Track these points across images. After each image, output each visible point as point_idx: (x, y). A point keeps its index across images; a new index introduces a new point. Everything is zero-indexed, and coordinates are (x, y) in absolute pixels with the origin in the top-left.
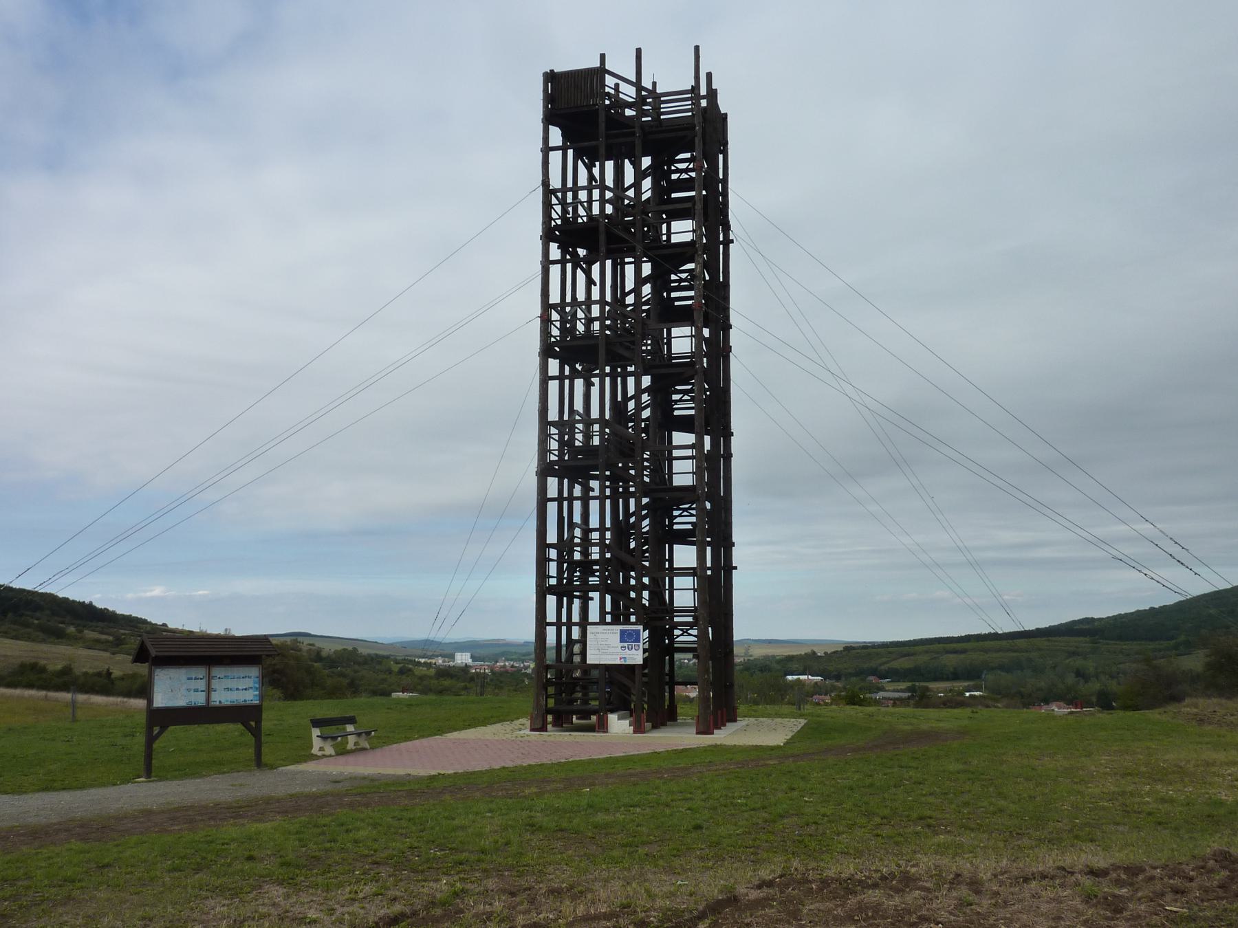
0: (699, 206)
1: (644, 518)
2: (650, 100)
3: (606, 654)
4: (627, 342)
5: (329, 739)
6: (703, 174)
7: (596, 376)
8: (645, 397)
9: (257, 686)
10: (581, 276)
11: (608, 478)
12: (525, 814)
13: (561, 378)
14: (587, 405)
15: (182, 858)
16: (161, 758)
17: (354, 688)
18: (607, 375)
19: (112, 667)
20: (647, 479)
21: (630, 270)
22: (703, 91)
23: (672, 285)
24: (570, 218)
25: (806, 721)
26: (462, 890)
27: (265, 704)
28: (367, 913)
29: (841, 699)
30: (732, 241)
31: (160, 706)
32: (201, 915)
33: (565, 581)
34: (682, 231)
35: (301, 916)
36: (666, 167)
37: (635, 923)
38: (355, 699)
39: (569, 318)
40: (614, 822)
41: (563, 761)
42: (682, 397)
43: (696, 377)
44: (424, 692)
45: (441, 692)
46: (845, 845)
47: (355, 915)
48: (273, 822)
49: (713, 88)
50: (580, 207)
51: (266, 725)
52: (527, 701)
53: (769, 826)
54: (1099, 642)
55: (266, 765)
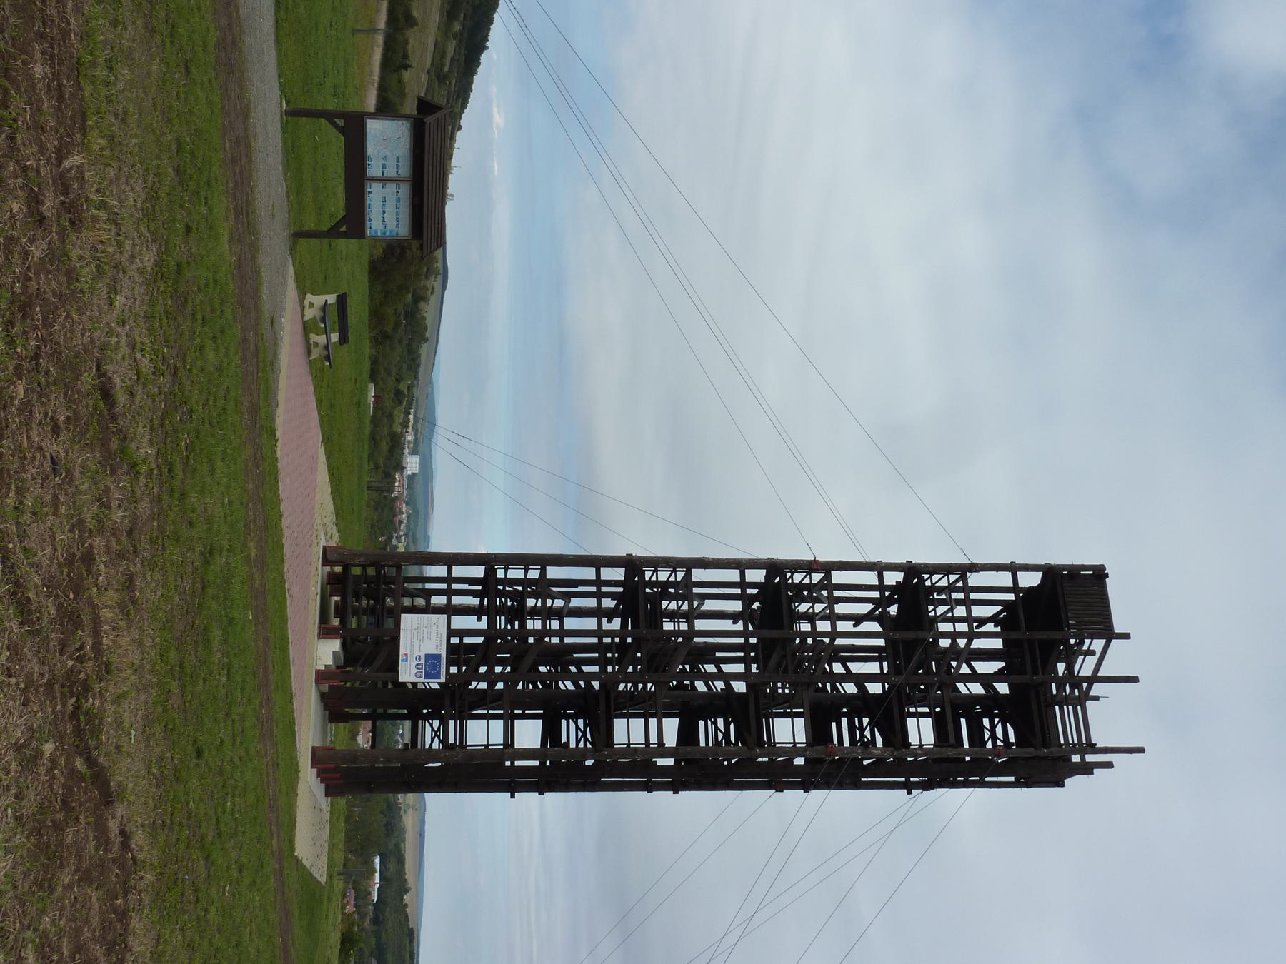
0: (951, 752)
1: (576, 684)
2: (1077, 693)
4: (787, 663)
5: (322, 314)
6: (990, 758)
7: (745, 626)
8: (720, 685)
9: (387, 234)
10: (865, 608)
11: (623, 640)
12: (226, 544)
13: (743, 584)
14: (710, 614)
15: (193, 153)
16: (308, 127)
17: (381, 338)
18: (747, 640)
19: (413, 70)
20: (621, 687)
21: (873, 667)
22: (1090, 758)
23: (856, 719)
24: (934, 596)
25: (323, 883)
26: (138, 473)
27: (365, 242)
28: (117, 363)
29: (349, 927)
30: (909, 793)
31: (368, 126)
32: (126, 176)
33: (501, 588)
34: (921, 731)
35: (118, 288)
36: (997, 711)
37: (86, 680)
38: (368, 340)
39: (814, 594)
40: (211, 651)
41: (287, 585)
42: (721, 731)
43: (745, 748)
44: (375, 421)
45: (373, 437)
46: (169, 940)
47: (116, 349)
48: (228, 252)
49: (1095, 770)
50: (947, 607)
51: (342, 243)
52: (358, 542)
53: (197, 841)
55: (295, 243)
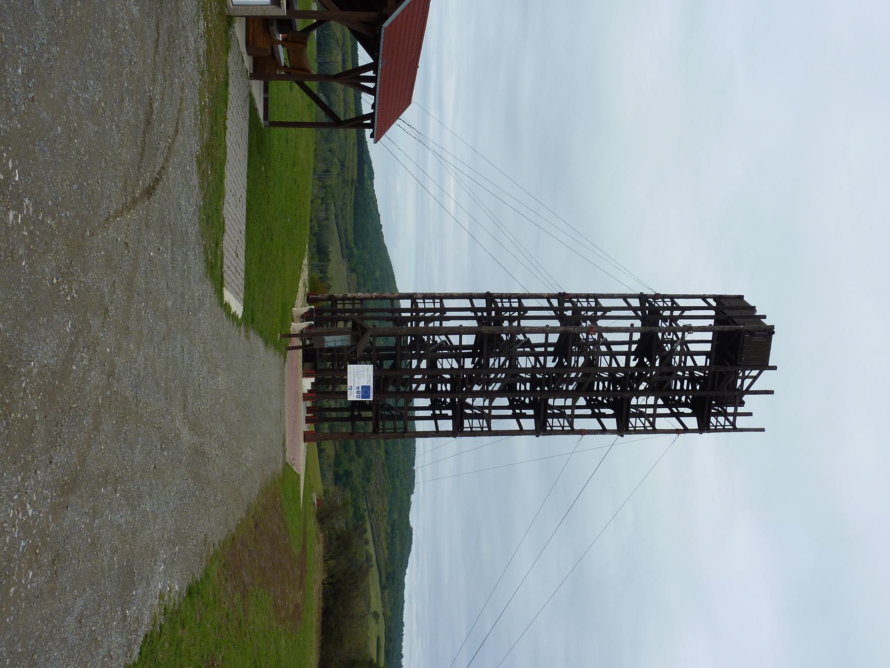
3: (354, 377)
54: (352, 186)
